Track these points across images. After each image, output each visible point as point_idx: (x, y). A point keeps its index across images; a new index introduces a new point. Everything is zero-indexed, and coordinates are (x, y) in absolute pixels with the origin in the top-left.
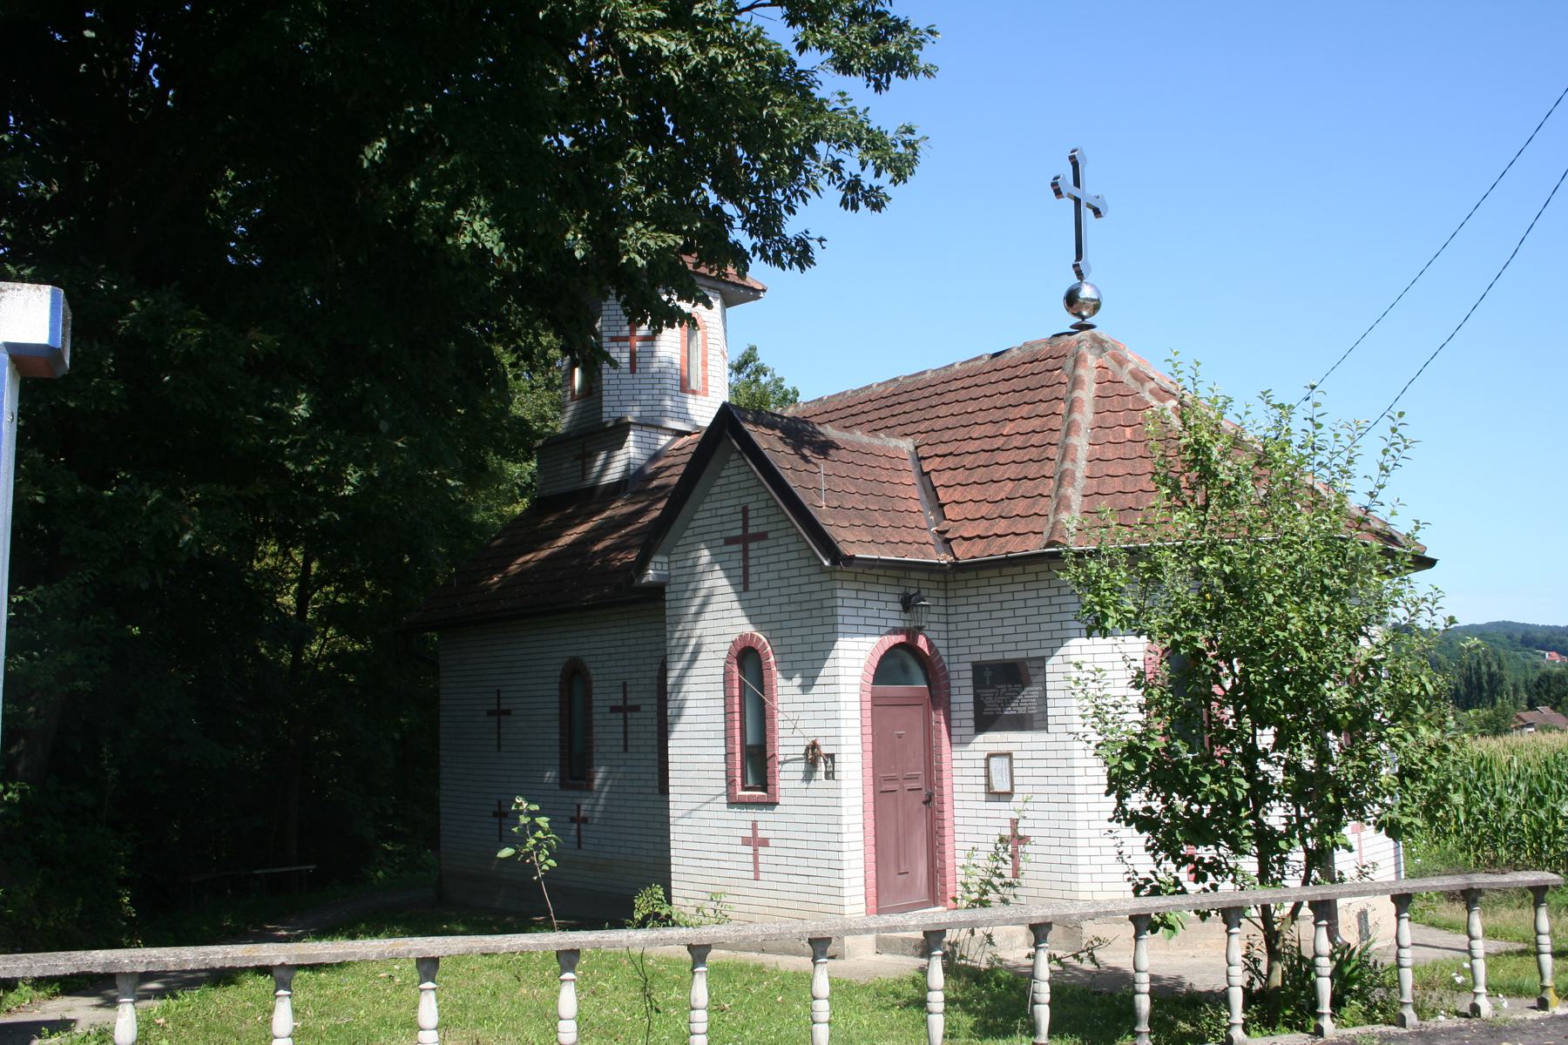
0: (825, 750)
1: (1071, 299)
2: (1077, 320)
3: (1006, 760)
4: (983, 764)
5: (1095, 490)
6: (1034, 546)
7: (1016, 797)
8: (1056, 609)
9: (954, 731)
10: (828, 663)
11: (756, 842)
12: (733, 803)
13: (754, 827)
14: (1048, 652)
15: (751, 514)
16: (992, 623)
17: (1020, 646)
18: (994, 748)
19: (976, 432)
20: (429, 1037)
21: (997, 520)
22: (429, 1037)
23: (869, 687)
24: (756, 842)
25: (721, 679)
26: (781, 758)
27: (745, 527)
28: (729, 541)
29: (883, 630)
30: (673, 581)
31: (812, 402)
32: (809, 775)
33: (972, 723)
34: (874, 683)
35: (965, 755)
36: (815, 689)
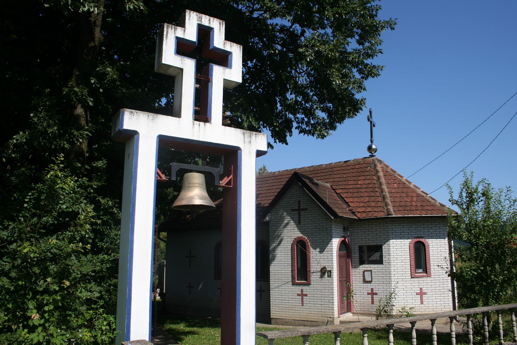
0: (328, 269)
1: (370, 148)
2: (371, 154)
3: (370, 272)
4: (362, 273)
5: (393, 200)
6: (382, 215)
7: (373, 282)
8: (386, 232)
9: (353, 264)
10: (329, 245)
11: (302, 295)
12: (294, 284)
13: (302, 291)
14: (383, 243)
15: (301, 203)
16: (365, 235)
17: (374, 241)
18: (366, 269)
19: (350, 183)
20: (435, 343)
21: (361, 208)
22: (435, 343)
23: (338, 252)
24: (302, 295)
25: (290, 249)
26: (312, 271)
27: (299, 206)
28: (293, 210)
29: (340, 236)
30: (272, 220)
31: (284, 171)
32: (322, 276)
33: (358, 262)
34: (339, 251)
35: (356, 271)
36: (324, 252)
